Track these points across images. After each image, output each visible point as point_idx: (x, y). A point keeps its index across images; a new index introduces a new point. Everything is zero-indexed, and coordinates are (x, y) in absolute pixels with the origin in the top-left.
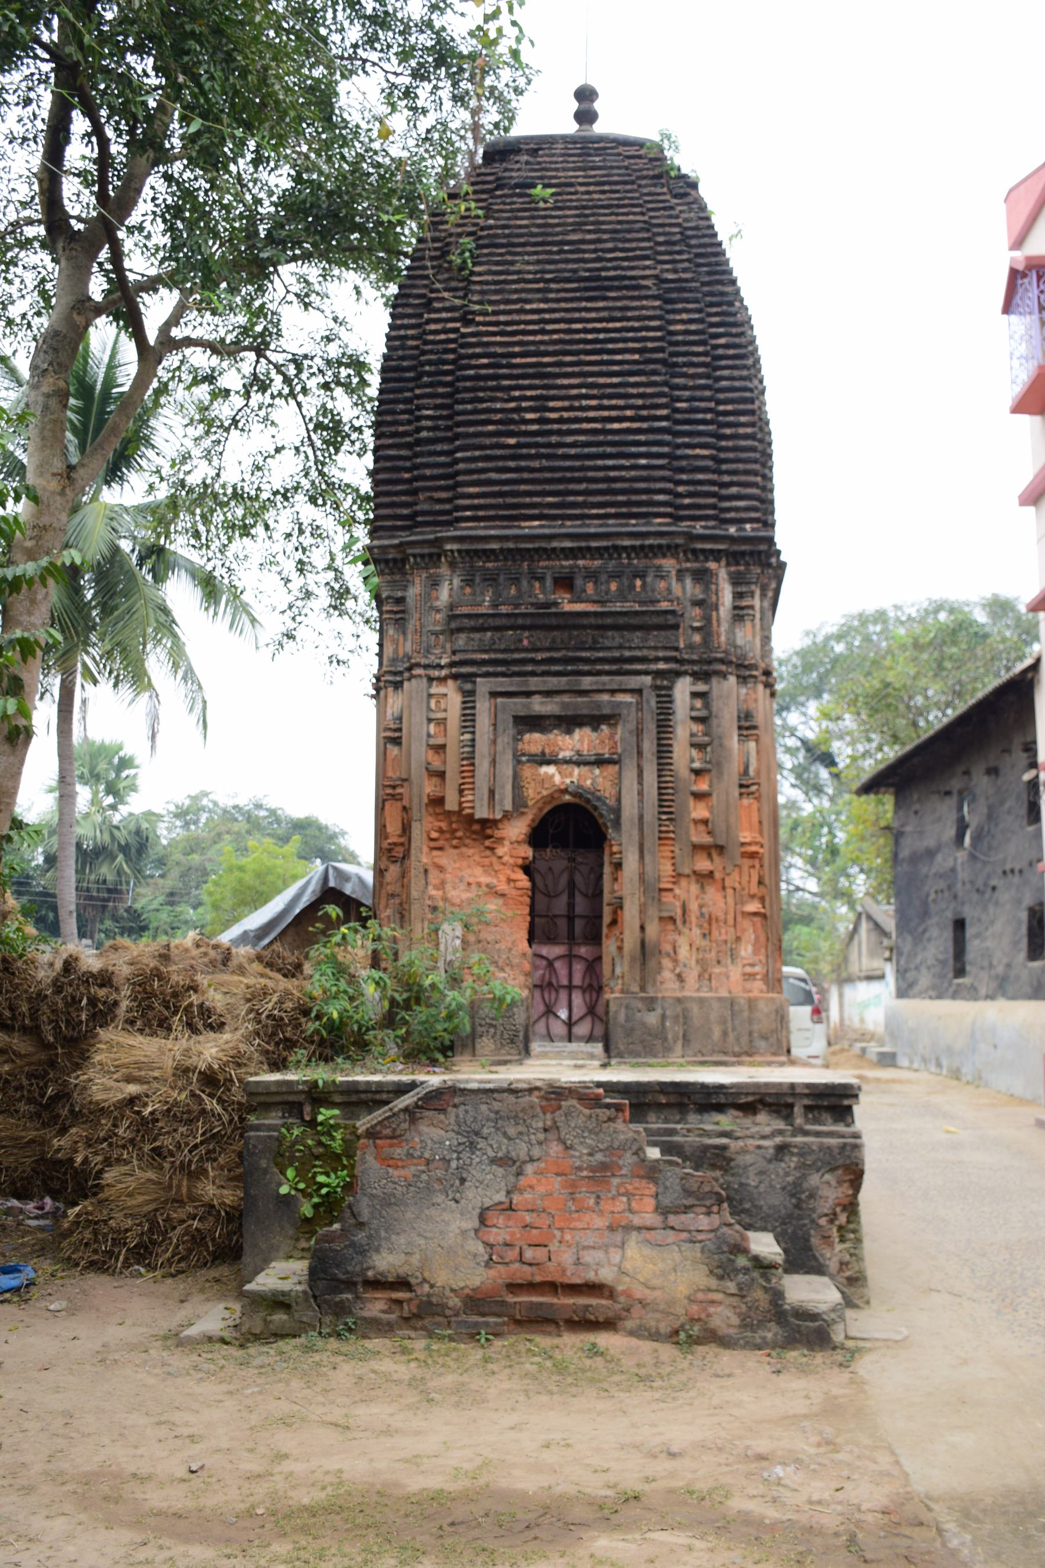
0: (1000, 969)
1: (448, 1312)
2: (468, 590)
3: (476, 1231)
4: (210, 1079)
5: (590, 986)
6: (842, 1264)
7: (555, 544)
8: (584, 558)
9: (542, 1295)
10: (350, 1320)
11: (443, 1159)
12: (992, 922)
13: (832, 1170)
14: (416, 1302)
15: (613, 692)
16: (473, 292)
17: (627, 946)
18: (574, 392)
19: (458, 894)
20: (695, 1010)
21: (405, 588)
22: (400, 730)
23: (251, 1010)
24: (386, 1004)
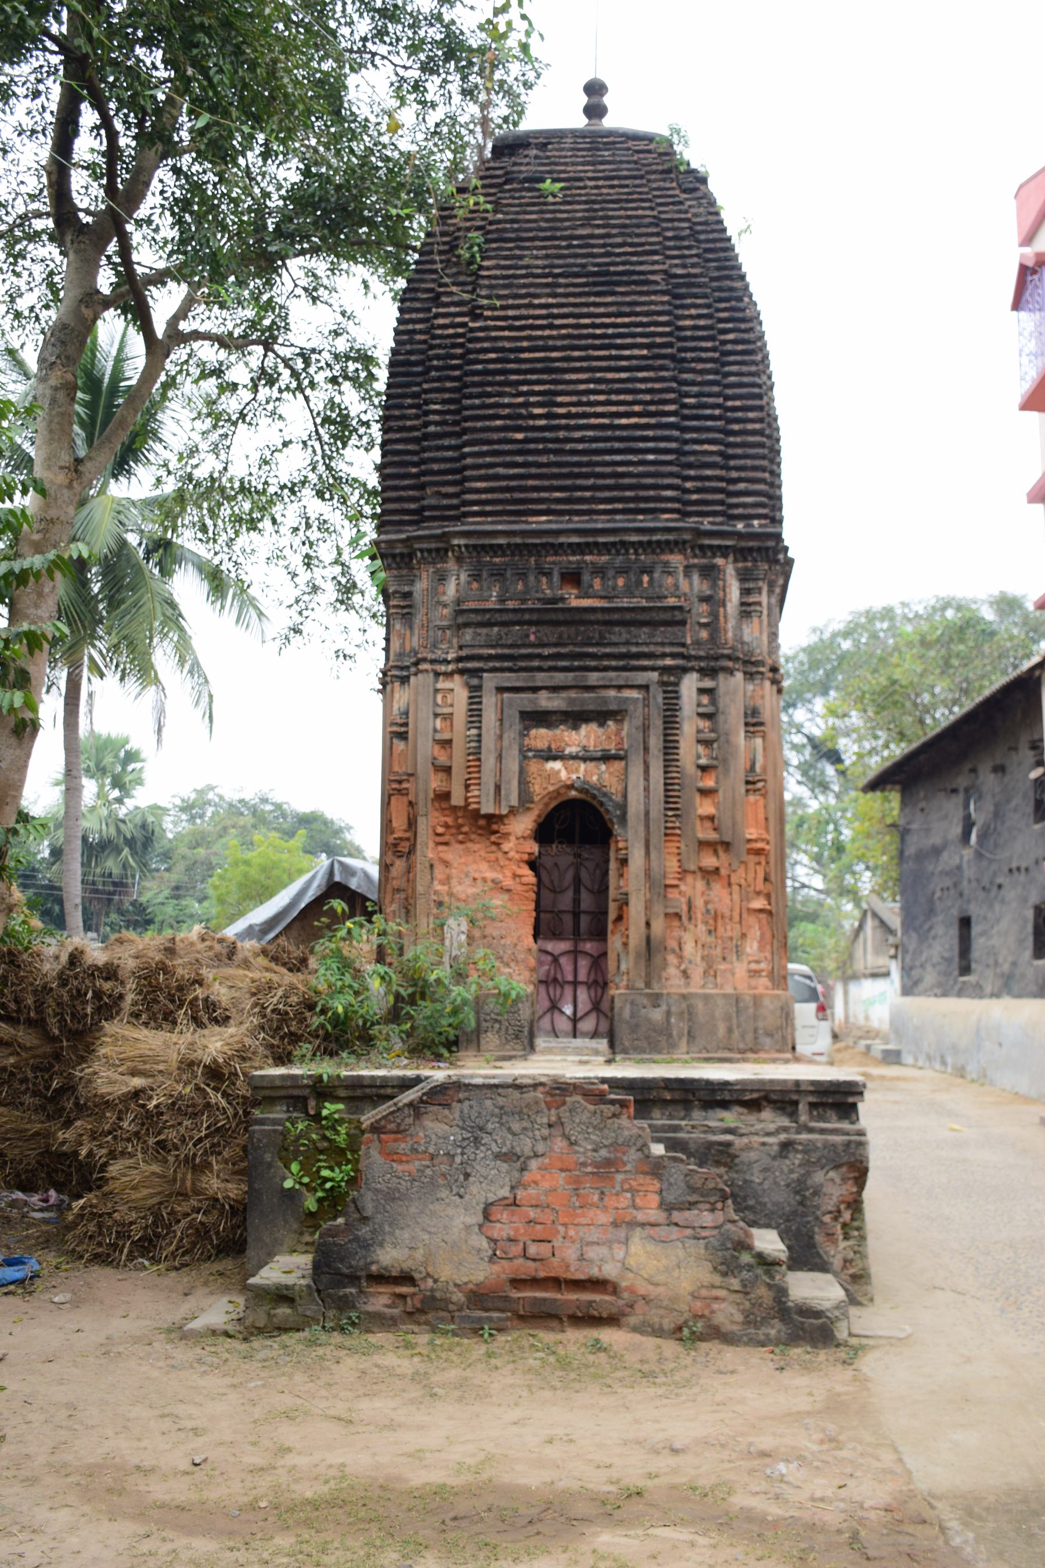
0: (1006, 967)
1: (451, 1307)
2: (475, 585)
3: (480, 1226)
4: (215, 1073)
5: (596, 982)
6: (845, 1261)
7: (562, 539)
8: (591, 553)
9: (546, 1290)
10: (353, 1315)
11: (447, 1154)
12: (998, 920)
13: (836, 1167)
15: (619, 688)
18: (583, 387)
19: (463, 889)
20: (700, 1005)
21: (412, 583)
22: (406, 724)
23: (256, 1005)
24: (391, 999)
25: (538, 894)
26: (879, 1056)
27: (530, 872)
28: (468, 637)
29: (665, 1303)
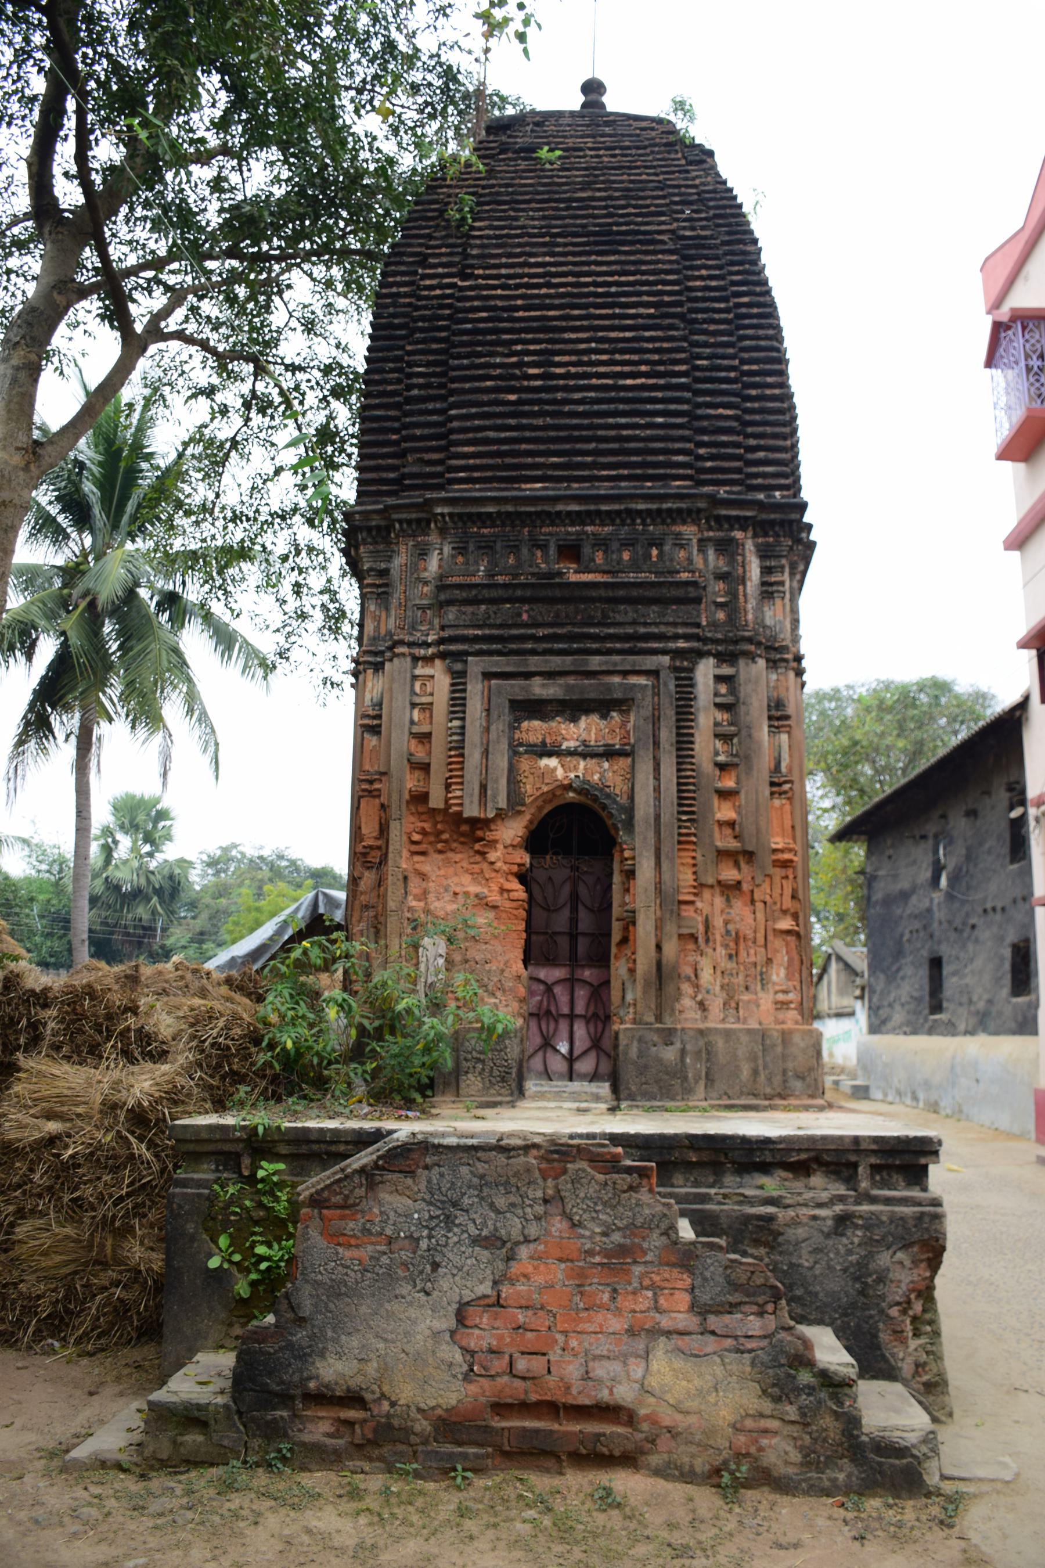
0: (981, 1005)
1: (413, 1439)
2: (460, 559)
3: (453, 1333)
4: (140, 1119)
5: (595, 1015)
6: (917, 1365)
7: (560, 507)
8: (593, 523)
9: (539, 1418)
10: (284, 1446)
11: (410, 1237)
12: (972, 960)
13: (905, 1247)
15: (625, 673)
16: (472, 247)
18: (583, 346)
19: (443, 906)
20: (720, 1043)
21: (389, 559)
22: (379, 717)
24: (353, 1032)
25: (529, 912)
26: (849, 1091)
28: (451, 616)
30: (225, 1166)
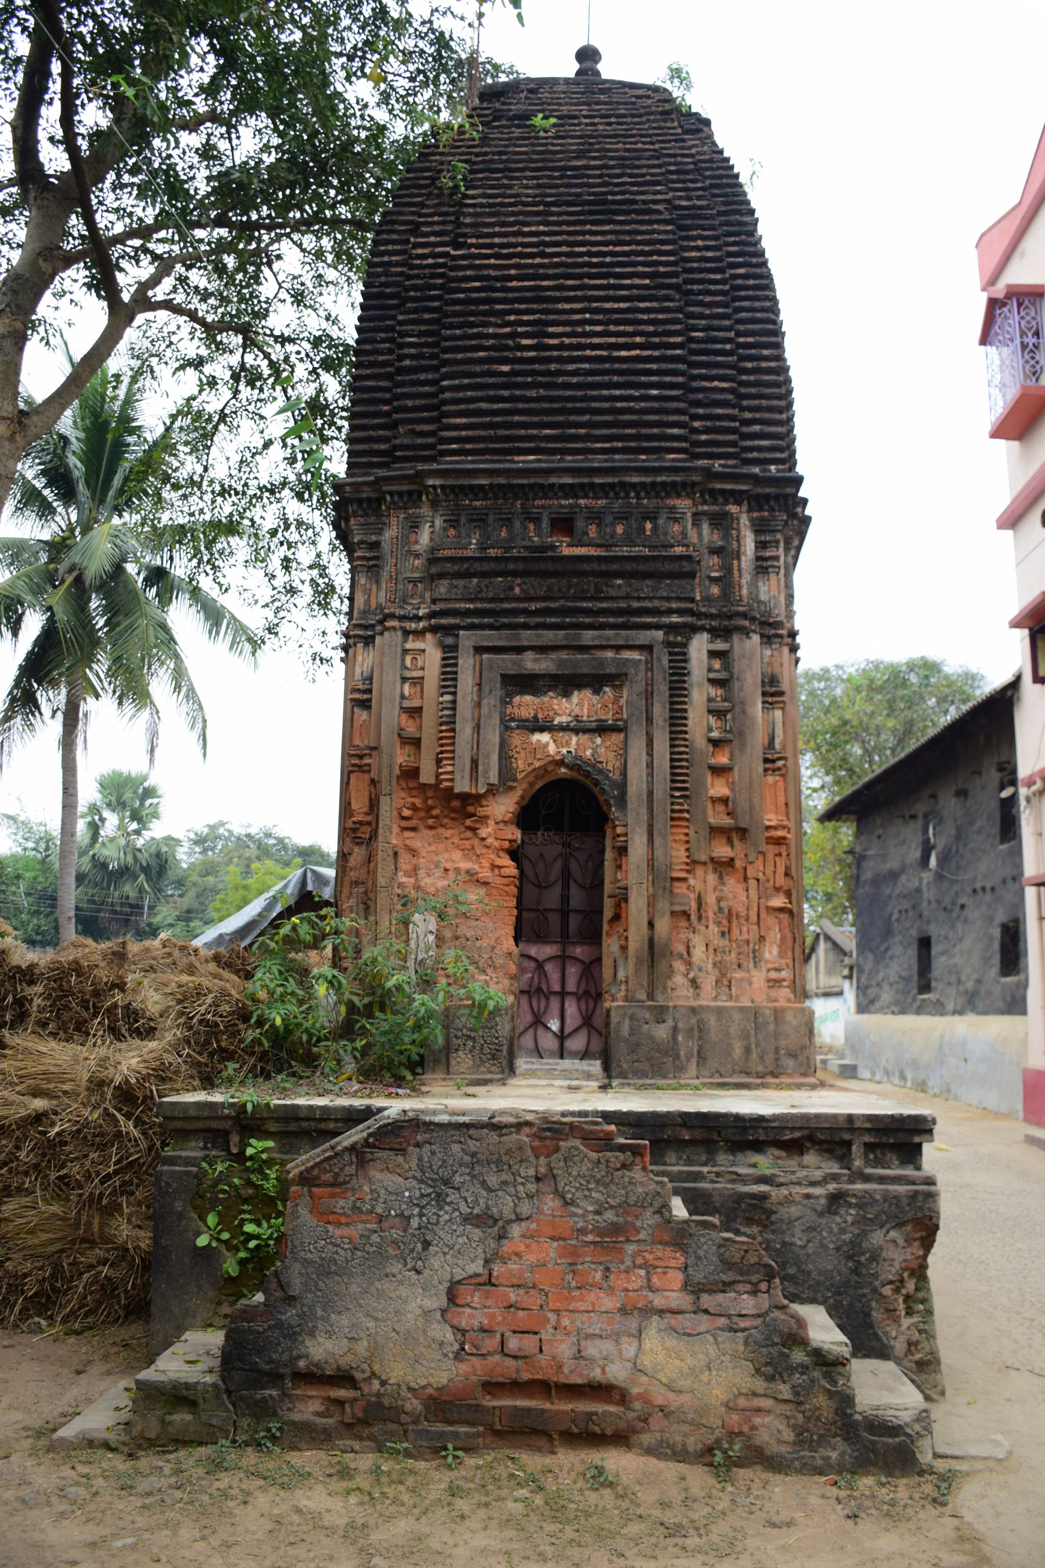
0: (970, 985)
1: (404, 1418)
2: (452, 532)
3: (444, 1312)
4: (127, 1096)
5: (587, 992)
6: (910, 1344)
7: (553, 480)
8: (586, 496)
10: (274, 1425)
11: (401, 1215)
12: (961, 940)
13: (898, 1226)
14: (361, 1403)
15: (618, 648)
17: (632, 945)
19: (433, 882)
20: (712, 1021)
21: (380, 532)
22: (369, 691)
23: (181, 1014)
24: (343, 1009)
25: (520, 889)
26: (836, 1070)
27: (511, 863)
28: (442, 590)
29: (690, 1416)
30: (214, 1143)
